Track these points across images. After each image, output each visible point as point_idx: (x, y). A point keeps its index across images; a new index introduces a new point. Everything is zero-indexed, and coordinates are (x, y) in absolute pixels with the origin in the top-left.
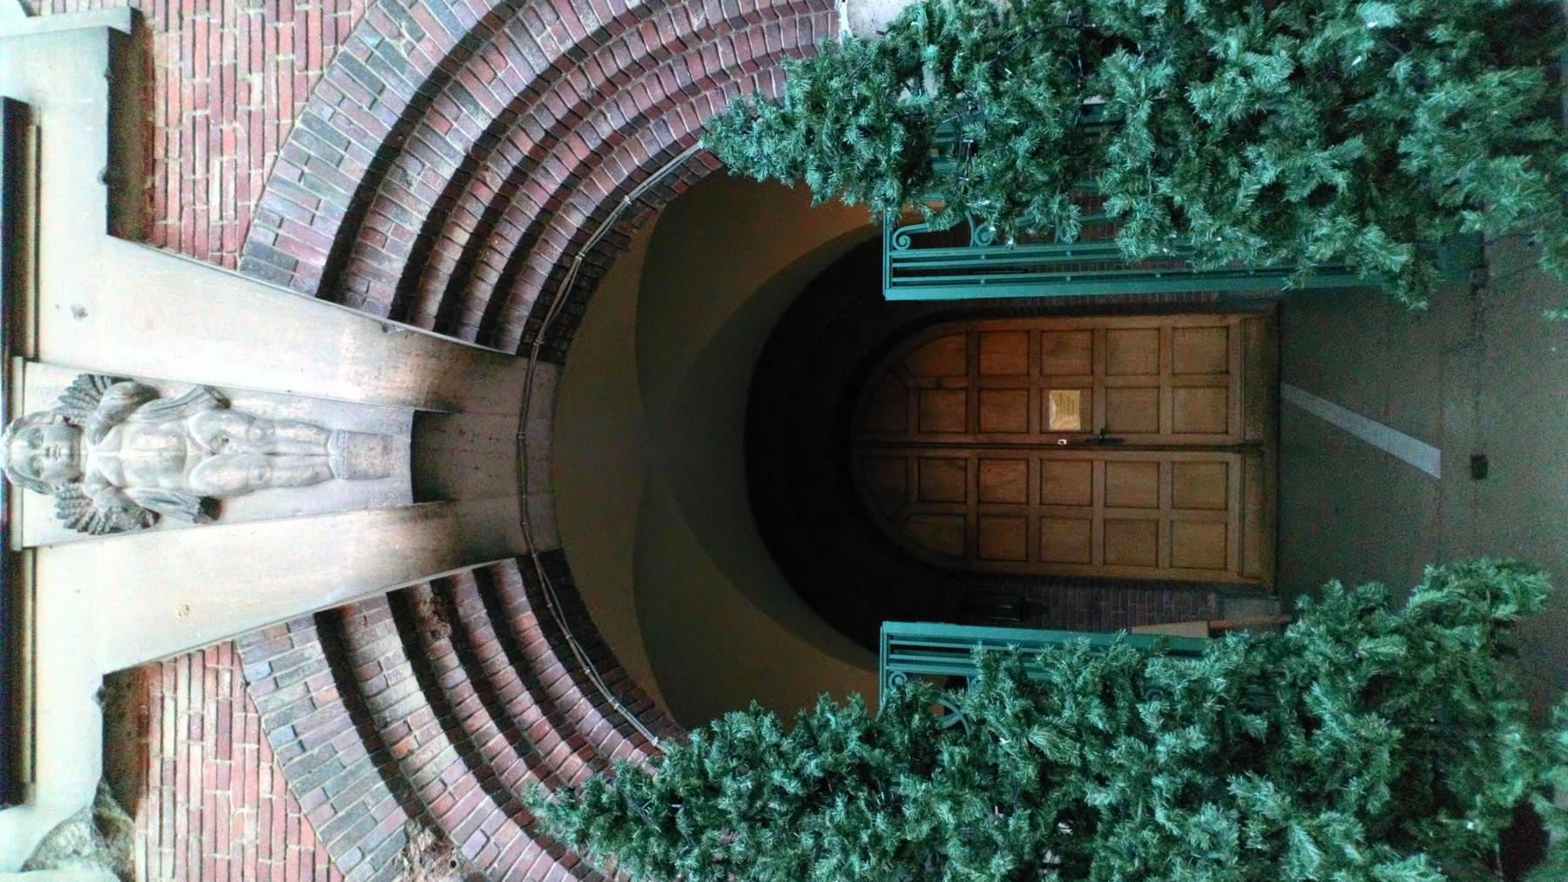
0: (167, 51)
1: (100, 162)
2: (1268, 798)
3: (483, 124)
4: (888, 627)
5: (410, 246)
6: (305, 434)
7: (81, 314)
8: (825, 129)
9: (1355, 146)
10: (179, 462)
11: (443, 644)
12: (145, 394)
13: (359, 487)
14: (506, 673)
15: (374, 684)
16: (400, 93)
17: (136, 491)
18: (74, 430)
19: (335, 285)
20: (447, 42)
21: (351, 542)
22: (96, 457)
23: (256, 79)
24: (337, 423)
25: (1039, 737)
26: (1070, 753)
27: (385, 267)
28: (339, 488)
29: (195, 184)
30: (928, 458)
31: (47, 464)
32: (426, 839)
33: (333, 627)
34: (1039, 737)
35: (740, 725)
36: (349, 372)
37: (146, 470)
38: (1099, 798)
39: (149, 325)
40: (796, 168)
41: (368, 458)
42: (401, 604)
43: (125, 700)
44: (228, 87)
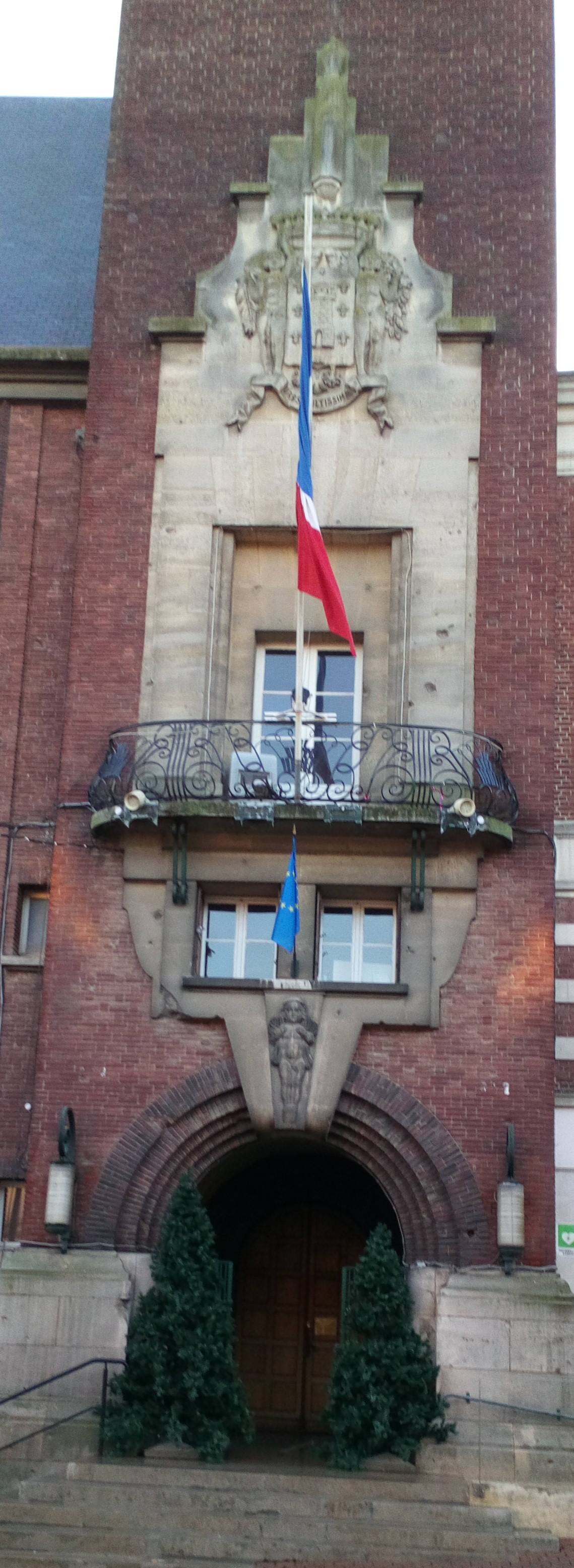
0: (424, 1039)
1: (387, 1021)
2: (205, 1368)
3: (395, 1145)
4: (231, 1265)
5: (358, 1118)
6: (297, 1097)
7: (339, 1012)
8: (374, 1265)
9: (350, 1396)
10: (289, 1057)
11: (231, 1121)
12: (311, 1043)
13: (281, 1113)
14: (220, 1140)
15: (219, 1102)
16: (405, 1121)
17: (282, 1042)
18: (300, 1021)
19: (345, 1094)
20: (419, 1139)
21: (263, 1103)
22: (291, 1028)
23: (413, 1070)
24: (300, 1106)
25: (213, 1317)
26: (209, 1325)
27: (352, 1109)
28: (280, 1106)
29: (379, 1054)
30: (530, 834)
31: (290, 1014)
32: (171, 1121)
33: (238, 1090)
34: (213, 1317)
35: (212, 1235)
36: (317, 1102)
37: (287, 1046)
38: (199, 1331)
39: (333, 1038)
40: (367, 1254)
41: (289, 1117)
42: (244, 1109)
43: (217, 1022)
44: (410, 1060)
